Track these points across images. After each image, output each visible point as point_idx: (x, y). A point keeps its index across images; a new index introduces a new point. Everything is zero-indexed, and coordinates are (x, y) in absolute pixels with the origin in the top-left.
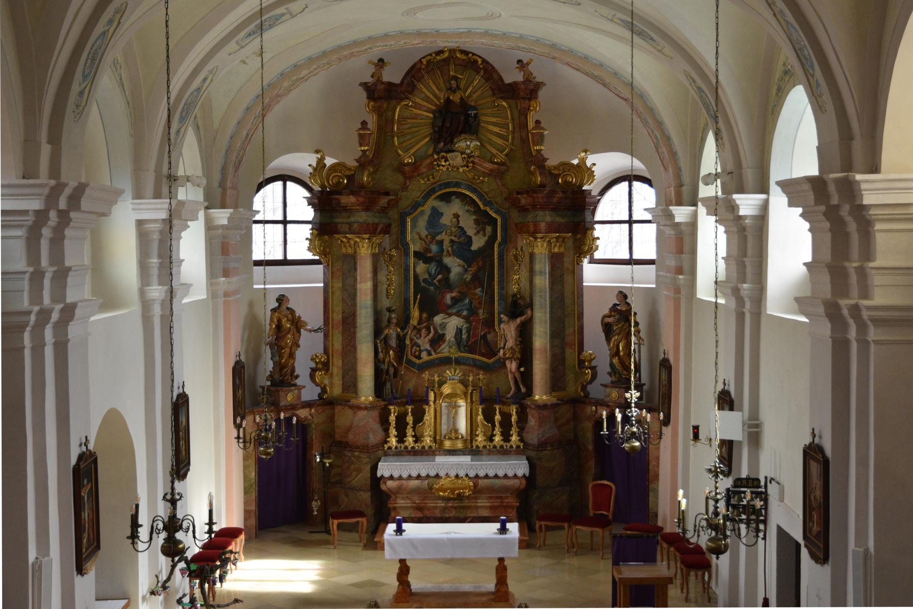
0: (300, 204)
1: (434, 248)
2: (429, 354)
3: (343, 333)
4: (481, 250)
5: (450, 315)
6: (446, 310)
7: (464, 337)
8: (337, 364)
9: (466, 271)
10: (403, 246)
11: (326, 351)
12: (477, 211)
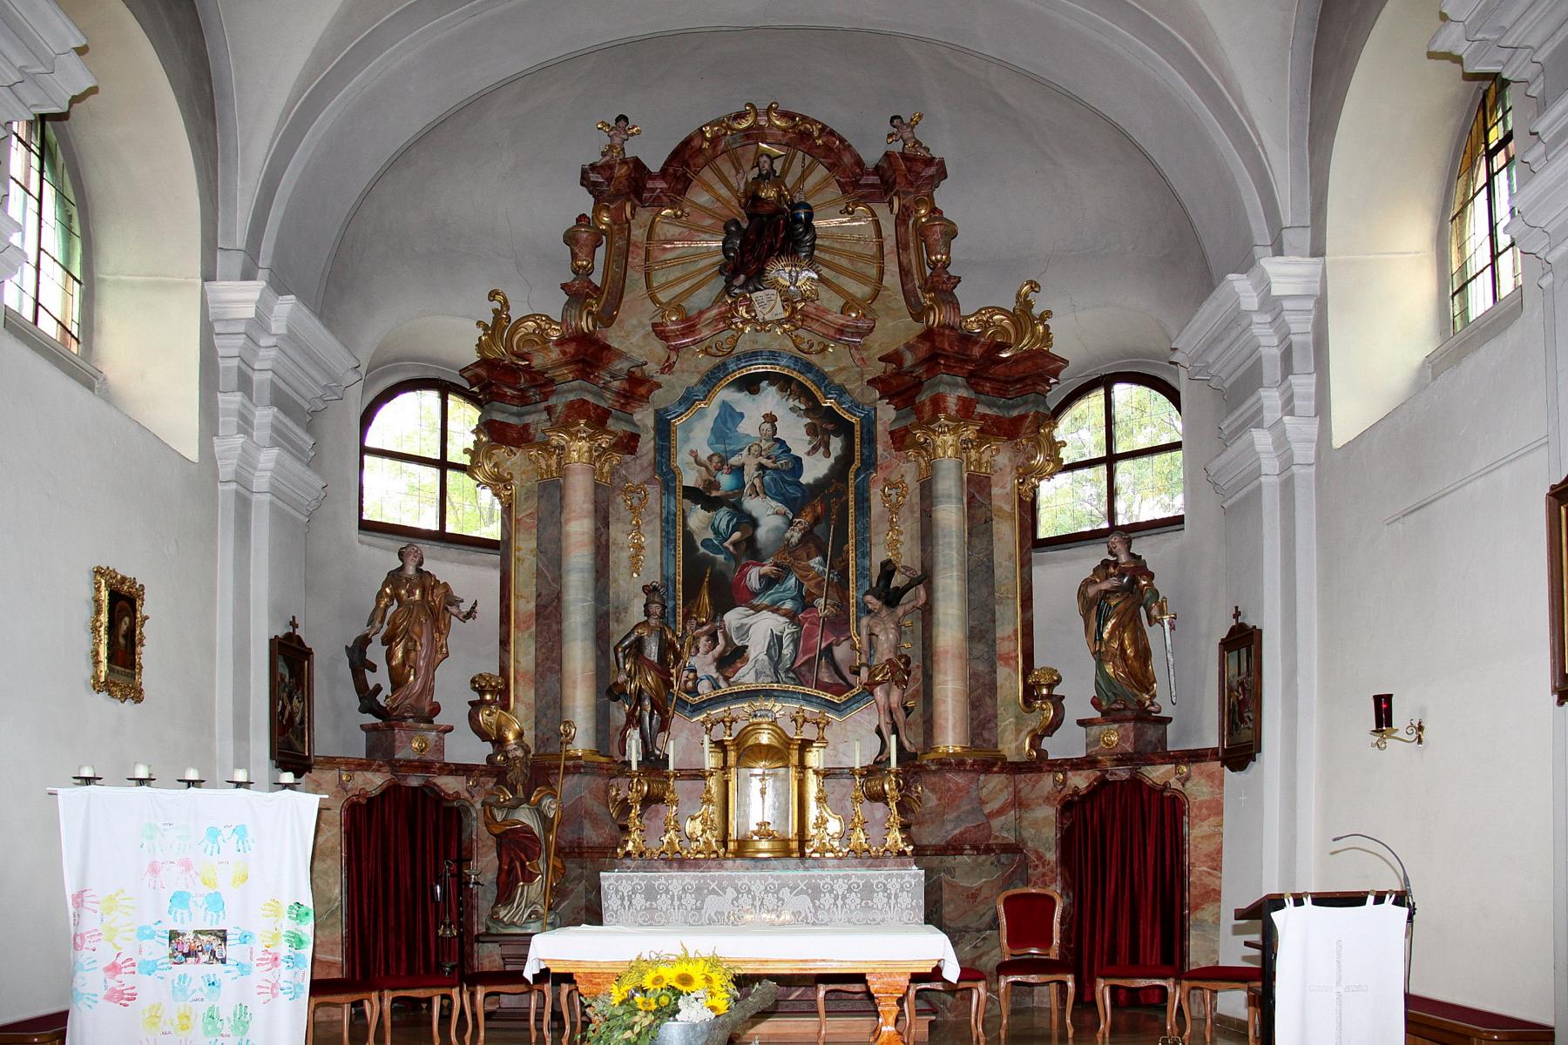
2: (715, 687)
3: (538, 634)
4: (820, 486)
7: (787, 651)
8: (523, 697)
9: (791, 523)
10: (665, 471)
11: (504, 671)
12: (813, 408)
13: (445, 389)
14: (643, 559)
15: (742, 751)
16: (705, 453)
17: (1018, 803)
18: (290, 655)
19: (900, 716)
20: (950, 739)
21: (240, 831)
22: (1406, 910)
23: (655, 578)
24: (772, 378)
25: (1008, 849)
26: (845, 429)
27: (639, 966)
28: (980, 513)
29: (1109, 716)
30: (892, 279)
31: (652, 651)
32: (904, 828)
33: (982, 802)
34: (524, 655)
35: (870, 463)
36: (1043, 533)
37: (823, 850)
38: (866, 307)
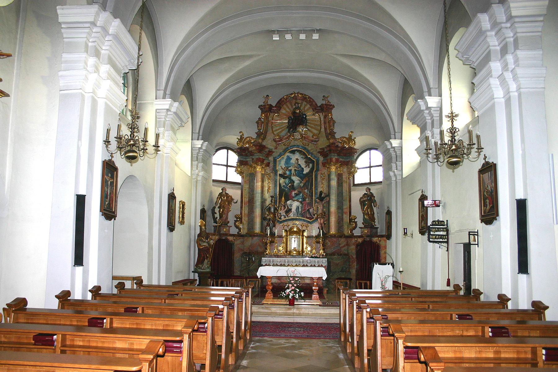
1: (288, 173)
2: (285, 217)
4: (307, 174)
5: (294, 201)
6: (292, 198)
8: (245, 219)
10: (275, 171)
11: (241, 213)
12: (306, 157)
13: (228, 148)
26: (313, 162)
29: (365, 227)
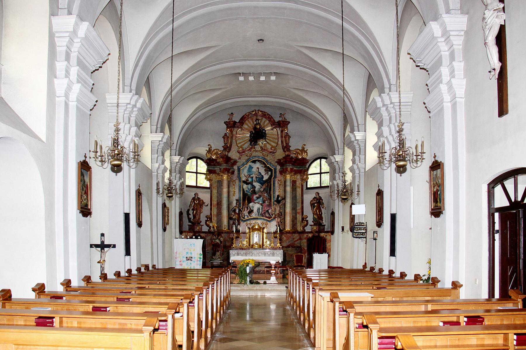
0: (203, 167)
3: (217, 208)
4: (267, 181)
8: (214, 219)
10: (240, 178)
11: (211, 214)
12: (266, 166)
14: (236, 195)
15: (253, 229)
16: (246, 174)
17: (300, 239)
18: (181, 214)
19: (280, 223)
20: (288, 228)
21: (194, 244)
22: (327, 255)
23: (237, 198)
24: (259, 161)
25: (298, 247)
26: (271, 170)
27: (244, 261)
28: (294, 187)
29: (315, 225)
30: (280, 142)
31: (237, 211)
32: (280, 243)
33: (294, 239)
34: (215, 211)
35: (275, 177)
36: (308, 186)
37: (266, 246)
38: (275, 148)
